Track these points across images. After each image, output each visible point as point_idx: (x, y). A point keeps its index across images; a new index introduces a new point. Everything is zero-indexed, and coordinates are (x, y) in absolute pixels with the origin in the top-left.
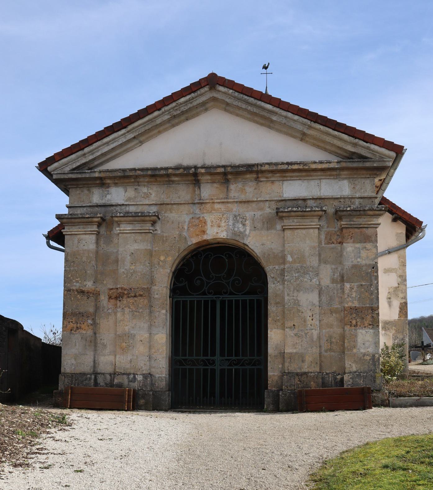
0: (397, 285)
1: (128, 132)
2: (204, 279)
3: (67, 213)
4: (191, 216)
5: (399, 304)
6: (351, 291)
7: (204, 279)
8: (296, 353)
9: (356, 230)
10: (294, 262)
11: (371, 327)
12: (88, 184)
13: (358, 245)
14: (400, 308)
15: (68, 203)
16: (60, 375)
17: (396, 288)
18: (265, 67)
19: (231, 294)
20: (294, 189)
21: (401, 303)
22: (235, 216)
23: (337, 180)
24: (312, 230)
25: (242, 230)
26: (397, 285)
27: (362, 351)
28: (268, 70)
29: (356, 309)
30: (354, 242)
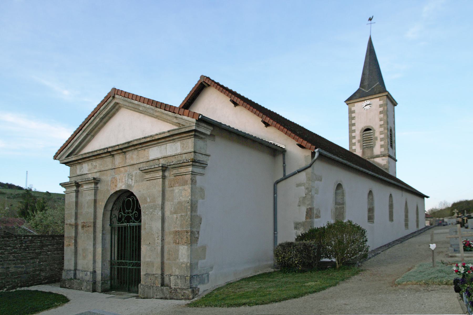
0: (304, 195)
1: (83, 132)
2: (123, 214)
3: (68, 181)
4: (112, 177)
5: (305, 210)
6: (176, 220)
7: (123, 214)
8: (150, 261)
9: (180, 177)
10: (150, 202)
11: (186, 244)
12: (80, 163)
13: (181, 188)
14: (307, 212)
15: (69, 175)
16: (63, 271)
17: (304, 198)
18: (370, 19)
19: (134, 222)
20: (154, 153)
21: (307, 209)
22: (129, 175)
23: (174, 143)
24: (159, 180)
25: (131, 183)
26: (304, 195)
27: (181, 261)
28: (373, 21)
29: (178, 232)
30: (179, 186)
